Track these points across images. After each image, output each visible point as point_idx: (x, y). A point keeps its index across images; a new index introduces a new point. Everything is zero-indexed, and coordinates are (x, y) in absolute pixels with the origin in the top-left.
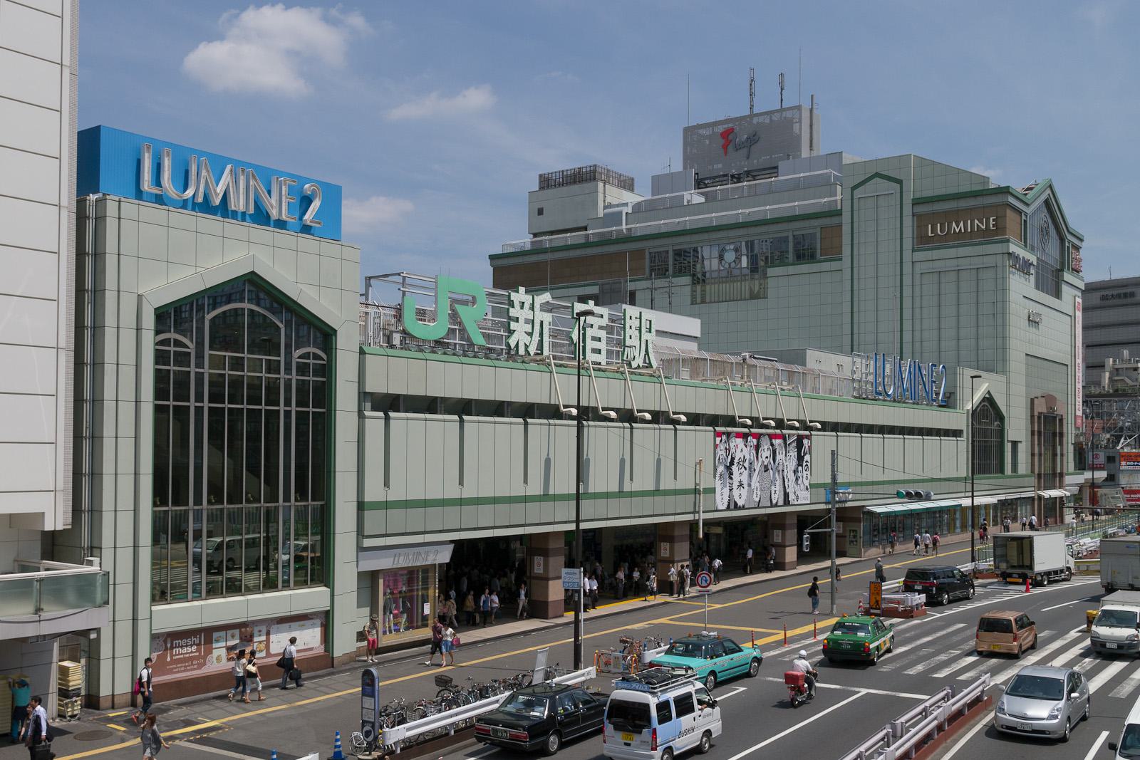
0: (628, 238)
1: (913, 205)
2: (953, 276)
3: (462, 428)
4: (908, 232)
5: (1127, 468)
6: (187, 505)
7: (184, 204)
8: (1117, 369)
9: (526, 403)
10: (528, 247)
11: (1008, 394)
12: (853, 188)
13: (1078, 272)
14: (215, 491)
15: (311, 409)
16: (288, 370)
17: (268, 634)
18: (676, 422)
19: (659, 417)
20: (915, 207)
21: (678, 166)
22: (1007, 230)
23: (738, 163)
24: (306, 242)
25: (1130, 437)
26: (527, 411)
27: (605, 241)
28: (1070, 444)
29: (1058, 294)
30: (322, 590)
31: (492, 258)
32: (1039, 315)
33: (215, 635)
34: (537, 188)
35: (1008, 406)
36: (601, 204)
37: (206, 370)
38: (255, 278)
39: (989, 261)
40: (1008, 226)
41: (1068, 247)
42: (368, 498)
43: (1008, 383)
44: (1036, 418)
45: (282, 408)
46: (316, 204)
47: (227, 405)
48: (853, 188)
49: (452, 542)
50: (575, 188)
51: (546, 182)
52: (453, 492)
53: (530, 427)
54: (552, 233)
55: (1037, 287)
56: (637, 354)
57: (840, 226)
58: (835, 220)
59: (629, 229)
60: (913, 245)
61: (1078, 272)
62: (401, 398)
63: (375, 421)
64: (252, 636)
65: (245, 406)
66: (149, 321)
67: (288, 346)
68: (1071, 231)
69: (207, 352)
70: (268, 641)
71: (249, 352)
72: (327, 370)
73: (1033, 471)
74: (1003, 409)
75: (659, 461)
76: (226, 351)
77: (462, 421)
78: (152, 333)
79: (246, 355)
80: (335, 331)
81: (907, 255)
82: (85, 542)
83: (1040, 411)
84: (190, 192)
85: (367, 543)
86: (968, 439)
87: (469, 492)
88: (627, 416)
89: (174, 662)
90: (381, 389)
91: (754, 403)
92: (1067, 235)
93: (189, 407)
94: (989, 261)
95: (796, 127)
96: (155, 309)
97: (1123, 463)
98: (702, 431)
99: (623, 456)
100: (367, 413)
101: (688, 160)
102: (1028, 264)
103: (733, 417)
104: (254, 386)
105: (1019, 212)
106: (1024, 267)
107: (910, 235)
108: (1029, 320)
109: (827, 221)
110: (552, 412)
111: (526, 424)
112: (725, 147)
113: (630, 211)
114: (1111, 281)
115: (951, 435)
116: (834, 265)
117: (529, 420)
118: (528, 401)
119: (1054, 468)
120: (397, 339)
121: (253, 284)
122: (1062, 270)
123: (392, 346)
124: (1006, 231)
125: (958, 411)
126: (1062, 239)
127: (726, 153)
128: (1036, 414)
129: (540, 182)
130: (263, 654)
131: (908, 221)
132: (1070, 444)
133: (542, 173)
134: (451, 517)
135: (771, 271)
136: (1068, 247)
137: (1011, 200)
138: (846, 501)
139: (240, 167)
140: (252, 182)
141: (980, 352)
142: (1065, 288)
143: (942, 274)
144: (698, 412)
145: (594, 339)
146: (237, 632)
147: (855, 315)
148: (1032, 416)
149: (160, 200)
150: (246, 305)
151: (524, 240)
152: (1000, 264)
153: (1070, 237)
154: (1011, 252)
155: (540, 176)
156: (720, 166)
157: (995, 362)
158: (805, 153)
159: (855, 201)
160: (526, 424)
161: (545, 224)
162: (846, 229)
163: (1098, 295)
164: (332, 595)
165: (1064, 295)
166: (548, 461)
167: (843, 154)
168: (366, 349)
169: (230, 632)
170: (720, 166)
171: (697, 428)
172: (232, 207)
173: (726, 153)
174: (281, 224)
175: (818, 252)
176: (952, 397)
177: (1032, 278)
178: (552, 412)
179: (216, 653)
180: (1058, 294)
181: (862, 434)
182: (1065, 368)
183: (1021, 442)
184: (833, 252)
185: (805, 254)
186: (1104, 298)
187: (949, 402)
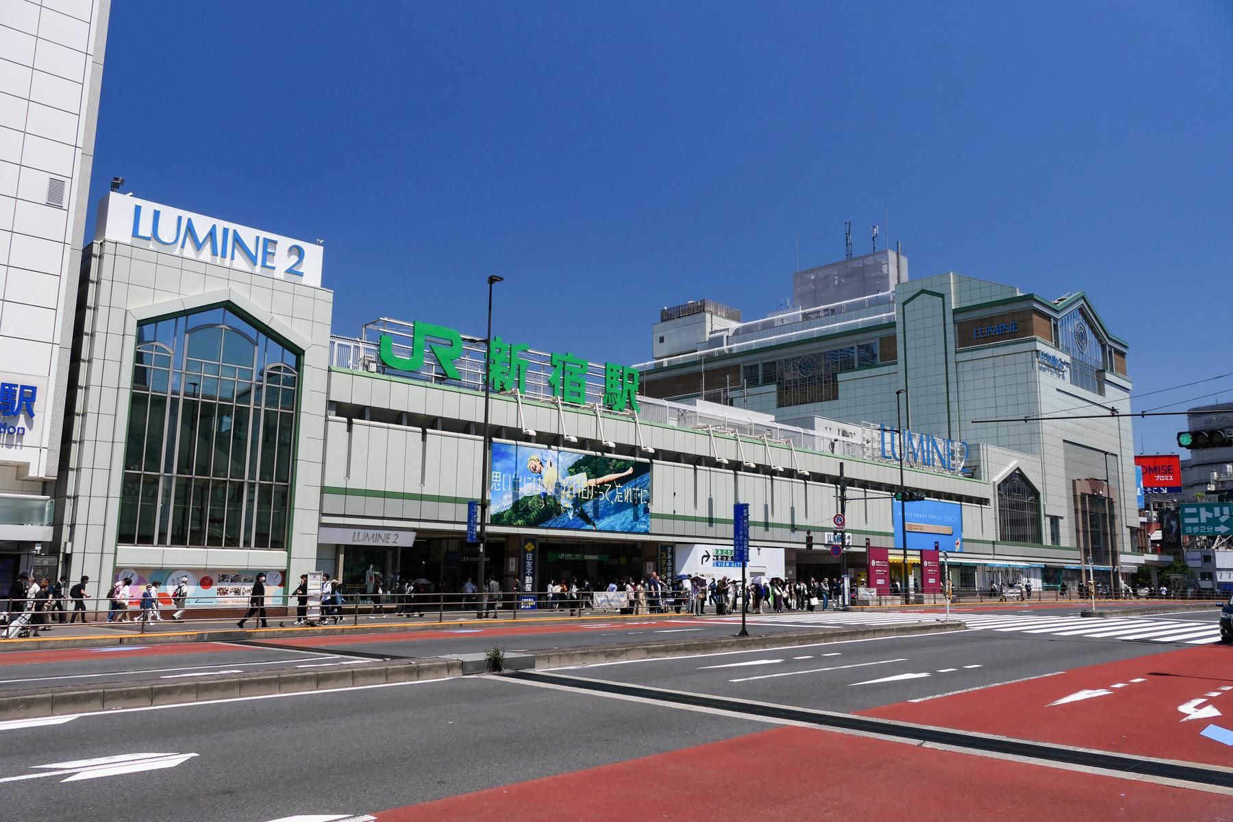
0: (731, 355)
1: (954, 314)
3: (424, 439)
4: (951, 337)
9: (696, 455)
11: (1044, 474)
12: (904, 304)
14: (185, 465)
19: (790, 473)
22: (1034, 331)
26: (696, 461)
28: (1124, 527)
29: (1101, 392)
35: (1044, 484)
36: (708, 330)
38: (230, 304)
40: (1034, 328)
41: (1110, 352)
43: (1043, 463)
45: (263, 407)
48: (904, 304)
49: (414, 530)
52: (415, 489)
55: (1074, 381)
56: (618, 400)
58: (891, 331)
59: (730, 350)
60: (956, 348)
62: (503, 430)
63: (338, 425)
66: (132, 329)
68: (1111, 337)
74: (1038, 487)
77: (736, 475)
85: (326, 520)
86: (995, 507)
87: (427, 491)
88: (736, 466)
90: (345, 399)
91: (793, 461)
92: (1108, 341)
95: (884, 268)
96: (138, 321)
98: (702, 470)
99: (710, 495)
100: (330, 417)
105: (1048, 318)
106: (1054, 366)
107: (953, 339)
109: (884, 333)
110: (711, 462)
111: (695, 469)
113: (730, 335)
115: (827, 480)
116: (892, 369)
117: (697, 467)
118: (427, 414)
122: (1103, 371)
124: (1033, 332)
125: (983, 481)
126: (1103, 347)
128: (1078, 493)
131: (950, 327)
134: (412, 509)
136: (1110, 352)
142: (1107, 386)
145: (572, 383)
148: (1075, 496)
153: (1110, 343)
160: (695, 469)
162: (900, 338)
164: (289, 558)
166: (710, 500)
171: (880, 492)
176: (978, 470)
177: (1067, 375)
178: (711, 462)
180: (1101, 392)
181: (982, 506)
182: (1115, 457)
183: (1062, 518)
187: (972, 472)
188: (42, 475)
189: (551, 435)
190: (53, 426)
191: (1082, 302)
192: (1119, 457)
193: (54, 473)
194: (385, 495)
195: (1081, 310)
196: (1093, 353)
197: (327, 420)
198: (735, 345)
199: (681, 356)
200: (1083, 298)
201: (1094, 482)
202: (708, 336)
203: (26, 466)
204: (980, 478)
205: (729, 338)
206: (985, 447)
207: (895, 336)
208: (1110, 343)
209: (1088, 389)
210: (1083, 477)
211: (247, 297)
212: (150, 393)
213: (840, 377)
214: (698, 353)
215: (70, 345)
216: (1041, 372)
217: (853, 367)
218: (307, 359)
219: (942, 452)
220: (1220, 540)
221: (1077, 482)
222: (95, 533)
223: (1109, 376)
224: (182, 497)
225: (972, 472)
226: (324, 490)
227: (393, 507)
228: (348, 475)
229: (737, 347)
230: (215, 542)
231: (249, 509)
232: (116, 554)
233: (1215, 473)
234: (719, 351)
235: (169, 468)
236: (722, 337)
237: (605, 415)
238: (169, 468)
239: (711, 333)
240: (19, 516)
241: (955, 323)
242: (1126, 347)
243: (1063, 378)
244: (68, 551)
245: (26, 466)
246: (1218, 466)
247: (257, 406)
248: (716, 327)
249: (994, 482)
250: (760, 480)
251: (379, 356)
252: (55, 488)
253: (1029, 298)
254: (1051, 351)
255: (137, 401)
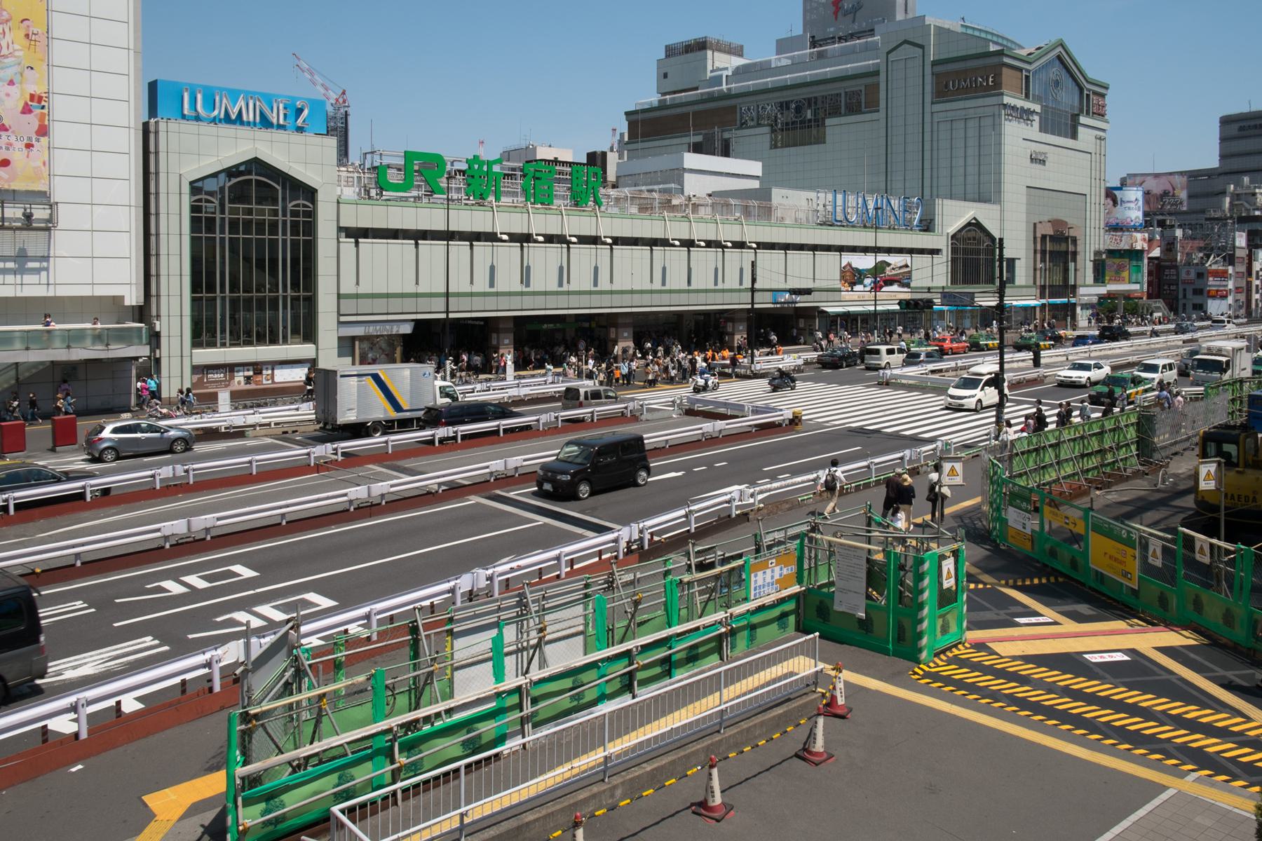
0: (728, 96)
2: (961, 124)
4: (928, 88)
5: (1214, 283)
6: (215, 293)
7: (214, 121)
8: (1238, 195)
10: (656, 104)
12: (888, 53)
13: (1103, 116)
14: (234, 287)
15: (301, 238)
16: (284, 215)
17: (273, 369)
18: (569, 243)
20: (934, 67)
21: (798, 30)
23: (845, 26)
24: (297, 137)
25: (1218, 256)
26: (653, 243)
27: (711, 98)
29: (1074, 136)
30: (312, 346)
31: (627, 113)
32: (1045, 154)
33: (236, 369)
34: (664, 57)
36: (709, 68)
37: (227, 215)
39: (989, 111)
42: (341, 292)
44: (1039, 240)
46: (306, 112)
47: (204, 235)
48: (888, 53)
49: (413, 320)
50: (690, 56)
51: (671, 51)
52: (411, 289)
53: (420, 246)
54: (675, 92)
57: (878, 84)
59: (729, 89)
61: (1103, 116)
64: (261, 370)
65: (254, 236)
66: (186, 189)
67: (284, 199)
69: (227, 205)
70: (273, 374)
71: (256, 204)
72: (312, 214)
73: (1035, 283)
75: (596, 269)
76: (239, 203)
78: (188, 196)
79: (254, 206)
80: (317, 190)
81: (928, 109)
82: (154, 313)
83: (1044, 233)
84: (216, 112)
85: (343, 319)
88: (689, 244)
89: (208, 382)
93: (215, 237)
94: (989, 111)
97: (1211, 279)
100: (341, 240)
101: (807, 24)
102: (1030, 112)
103: (693, 241)
104: (260, 224)
106: (1025, 115)
108: (1032, 159)
112: (836, 13)
113: (730, 73)
114: (1250, 112)
116: (874, 116)
119: (1066, 278)
120: (373, 193)
121: (256, 164)
122: (1078, 115)
123: (370, 198)
126: (1081, 89)
127: (836, 18)
128: (1039, 235)
129: (666, 51)
130: (270, 382)
131: (928, 79)
132: (1088, 262)
133: (667, 44)
134: (409, 305)
135: (828, 122)
137: (1006, 60)
138: (796, 303)
139: (249, 95)
140: (258, 103)
141: (981, 186)
143: (954, 122)
144: (654, 237)
146: (251, 368)
147: (889, 156)
148: (1035, 238)
149: (198, 118)
150: (253, 177)
151: (652, 98)
152: (997, 113)
153: (1089, 86)
154: (1005, 103)
155: (666, 46)
156: (832, 29)
157: (987, 193)
158: (900, 16)
159: (890, 63)
161: (669, 85)
163: (1236, 126)
164: (317, 349)
165: (1080, 136)
166: (492, 268)
167: (926, 18)
168: (340, 201)
169: (246, 368)
170: (832, 29)
172: (245, 118)
173: (836, 18)
174: (280, 127)
175: (863, 106)
178: (665, 243)
179: (237, 379)
180: (1074, 136)
183: (1019, 259)
184: (873, 106)
185: (854, 109)
186: (1241, 129)
187: (927, 226)
188: (134, 304)
189: (522, 234)
190: (137, 266)
191: (1060, 49)
192: (1088, 197)
193: (141, 301)
194: (388, 296)
195: (1059, 58)
196: (1068, 98)
197: (339, 242)
198: (733, 85)
199: (683, 94)
200: (1062, 45)
201: (1056, 223)
202: (709, 75)
203: (122, 298)
204: (934, 232)
205: (729, 78)
206: (940, 202)
207: (878, 84)
208: (1089, 86)
209: (1059, 135)
210: (1046, 218)
211: (270, 153)
212: (203, 215)
213: (828, 122)
214: (699, 91)
215: (141, 204)
216: (1007, 123)
217: (840, 113)
218: (320, 196)
219: (896, 209)
220: (1214, 257)
221: (1038, 226)
222: (175, 342)
223: (1083, 120)
224: (234, 250)
225: (927, 226)
226: (339, 296)
227: (396, 305)
228: (358, 283)
229: (735, 87)
230: (261, 340)
231: (284, 316)
232: (191, 356)
233: (1232, 186)
234: (718, 91)
235: (223, 291)
236: (721, 76)
237: (570, 213)
238: (223, 291)
239: (712, 72)
240: (123, 337)
241: (933, 74)
242: (1107, 88)
243: (1032, 126)
244: (158, 356)
245: (122, 298)
246: (1235, 177)
247: (284, 238)
248: (717, 64)
249: (948, 234)
250: (712, 254)
251: (377, 183)
252: (142, 313)
253: (1000, 53)
254: (1019, 103)
255: (195, 223)
